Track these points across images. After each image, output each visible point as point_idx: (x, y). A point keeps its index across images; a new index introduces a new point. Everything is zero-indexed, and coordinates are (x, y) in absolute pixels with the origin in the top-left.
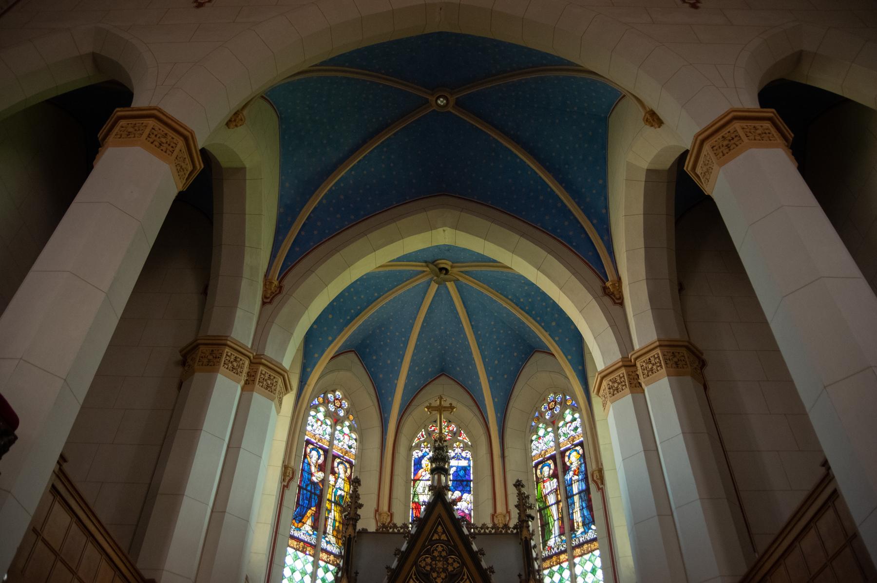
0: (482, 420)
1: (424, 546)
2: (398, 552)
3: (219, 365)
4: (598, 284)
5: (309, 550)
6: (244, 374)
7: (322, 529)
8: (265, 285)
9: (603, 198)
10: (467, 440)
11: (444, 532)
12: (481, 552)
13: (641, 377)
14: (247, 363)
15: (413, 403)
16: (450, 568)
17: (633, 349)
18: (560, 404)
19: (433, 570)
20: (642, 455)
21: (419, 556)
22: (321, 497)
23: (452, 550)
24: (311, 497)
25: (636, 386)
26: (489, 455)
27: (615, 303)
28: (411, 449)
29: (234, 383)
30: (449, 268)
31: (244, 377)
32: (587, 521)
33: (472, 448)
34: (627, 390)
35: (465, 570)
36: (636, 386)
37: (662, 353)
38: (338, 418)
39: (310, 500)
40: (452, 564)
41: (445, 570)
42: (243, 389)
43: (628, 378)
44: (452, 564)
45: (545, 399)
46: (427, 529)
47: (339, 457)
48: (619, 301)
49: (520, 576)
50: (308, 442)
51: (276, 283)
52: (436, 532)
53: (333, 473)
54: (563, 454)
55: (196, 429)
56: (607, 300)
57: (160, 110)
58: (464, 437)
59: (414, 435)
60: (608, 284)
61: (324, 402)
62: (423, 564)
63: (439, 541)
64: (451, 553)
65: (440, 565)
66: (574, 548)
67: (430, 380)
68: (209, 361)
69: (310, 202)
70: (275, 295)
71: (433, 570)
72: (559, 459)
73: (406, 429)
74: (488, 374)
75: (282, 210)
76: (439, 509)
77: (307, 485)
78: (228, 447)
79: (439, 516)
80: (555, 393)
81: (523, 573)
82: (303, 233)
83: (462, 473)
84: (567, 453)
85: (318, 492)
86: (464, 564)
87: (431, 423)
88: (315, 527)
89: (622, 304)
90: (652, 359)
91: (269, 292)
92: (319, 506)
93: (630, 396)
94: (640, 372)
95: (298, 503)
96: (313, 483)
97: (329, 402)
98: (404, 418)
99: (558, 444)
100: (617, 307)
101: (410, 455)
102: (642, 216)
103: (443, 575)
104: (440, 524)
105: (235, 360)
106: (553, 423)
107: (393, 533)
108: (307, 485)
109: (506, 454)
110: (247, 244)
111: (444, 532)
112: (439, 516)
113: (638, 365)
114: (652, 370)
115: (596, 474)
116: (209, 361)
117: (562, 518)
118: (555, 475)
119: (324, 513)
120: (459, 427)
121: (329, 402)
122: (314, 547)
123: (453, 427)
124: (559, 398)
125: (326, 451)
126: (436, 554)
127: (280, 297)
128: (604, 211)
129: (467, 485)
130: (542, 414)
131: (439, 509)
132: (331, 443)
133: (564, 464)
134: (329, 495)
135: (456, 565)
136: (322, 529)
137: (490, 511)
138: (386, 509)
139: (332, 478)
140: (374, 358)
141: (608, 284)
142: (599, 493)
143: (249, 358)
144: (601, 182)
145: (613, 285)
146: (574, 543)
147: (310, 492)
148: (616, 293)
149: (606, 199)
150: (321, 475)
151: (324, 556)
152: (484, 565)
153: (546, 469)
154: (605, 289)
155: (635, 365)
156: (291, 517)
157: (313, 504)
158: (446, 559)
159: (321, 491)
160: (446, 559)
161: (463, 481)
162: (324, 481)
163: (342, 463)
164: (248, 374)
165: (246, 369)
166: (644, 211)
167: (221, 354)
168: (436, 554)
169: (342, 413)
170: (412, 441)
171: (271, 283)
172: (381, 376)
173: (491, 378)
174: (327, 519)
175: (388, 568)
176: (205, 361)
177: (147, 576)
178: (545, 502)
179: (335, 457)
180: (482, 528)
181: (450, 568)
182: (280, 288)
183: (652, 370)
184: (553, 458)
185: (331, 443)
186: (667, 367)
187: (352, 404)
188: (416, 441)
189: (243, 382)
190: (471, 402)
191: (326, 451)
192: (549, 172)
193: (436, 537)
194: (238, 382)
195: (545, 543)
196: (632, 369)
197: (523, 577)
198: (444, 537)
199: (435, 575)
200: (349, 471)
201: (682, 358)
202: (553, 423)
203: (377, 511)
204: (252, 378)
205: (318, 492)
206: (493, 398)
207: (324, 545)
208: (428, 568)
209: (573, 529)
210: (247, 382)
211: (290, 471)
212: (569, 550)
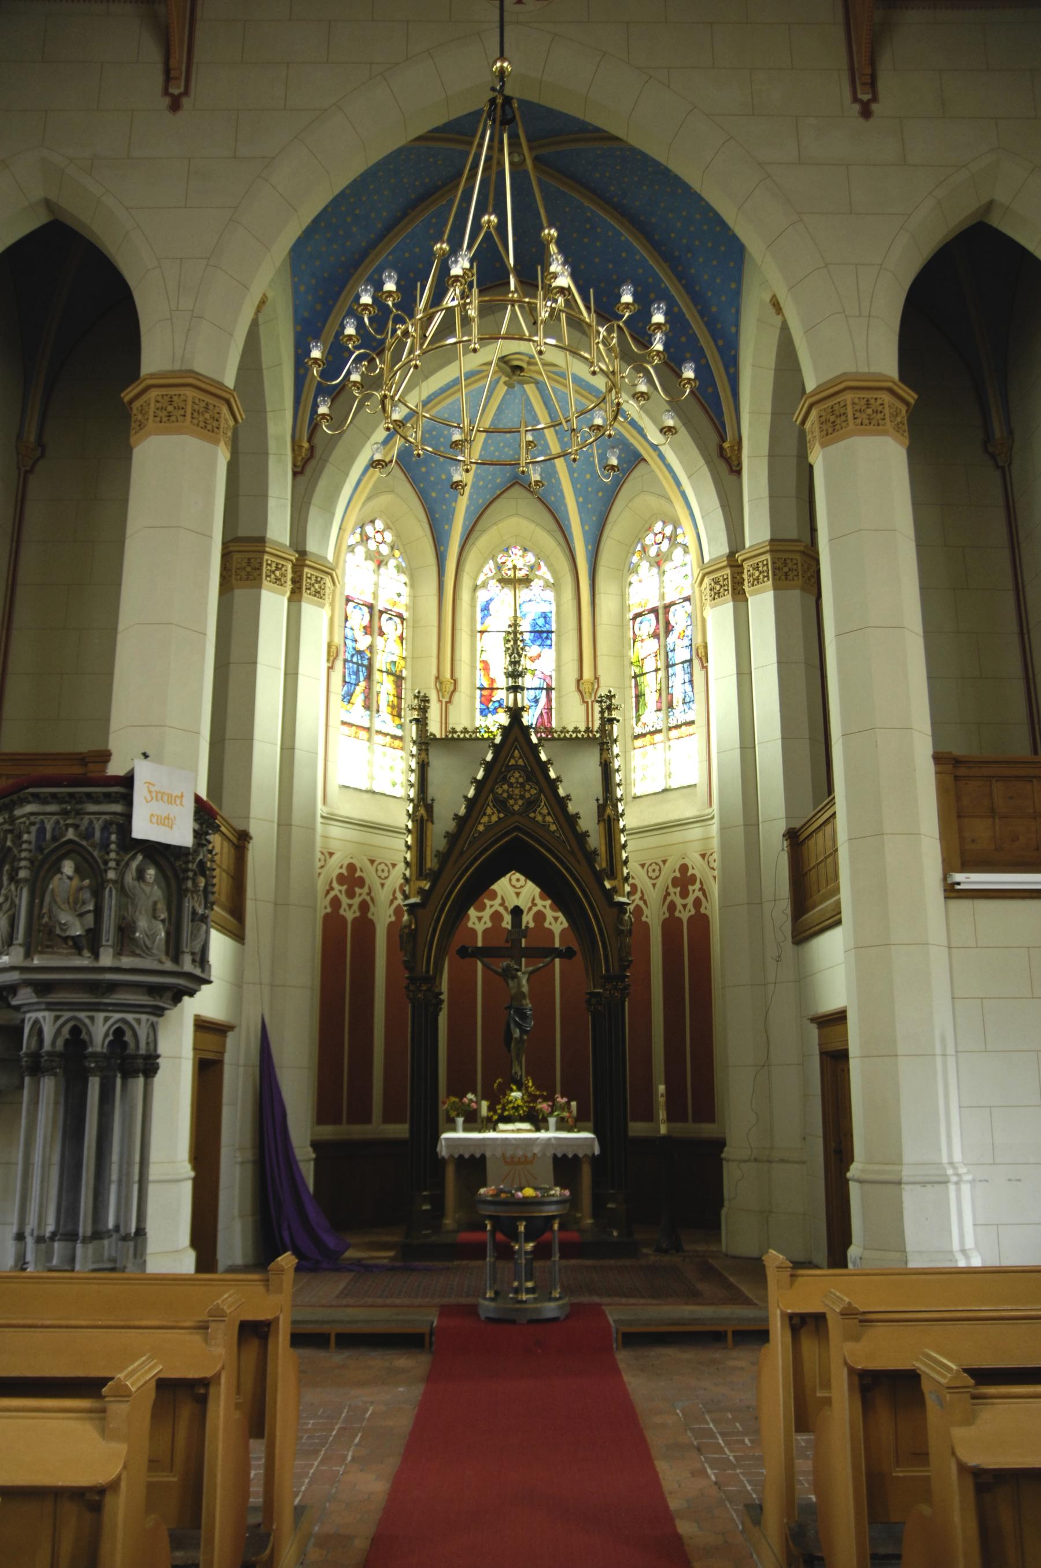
0: (567, 551)
1: (500, 772)
2: (475, 780)
3: (261, 579)
4: (713, 439)
5: (364, 734)
6: (289, 583)
7: (375, 708)
8: (293, 450)
9: (733, 310)
10: (549, 576)
11: (521, 757)
12: (558, 779)
13: (746, 582)
14: (289, 566)
15: (478, 527)
16: (527, 795)
17: (744, 548)
18: (670, 539)
19: (510, 797)
20: (735, 677)
21: (496, 783)
22: (370, 668)
23: (530, 777)
24: (358, 670)
25: (739, 595)
26: (575, 602)
27: (855, 99)
28: (475, 588)
29: (281, 597)
30: (524, 365)
31: (289, 586)
32: (688, 699)
33: (555, 586)
34: (729, 597)
35: (542, 796)
36: (739, 595)
37: (772, 559)
38: (381, 558)
39: (357, 673)
40: (529, 791)
41: (522, 797)
42: (290, 600)
43: (733, 581)
44: (529, 791)
45: (650, 529)
46: (503, 755)
47: (386, 611)
48: (736, 470)
49: (597, 800)
50: (348, 600)
51: (306, 445)
52: (512, 757)
53: (381, 633)
54: (667, 608)
55: (252, 662)
56: (723, 467)
57: (191, 371)
58: (544, 571)
59: (479, 571)
60: (726, 445)
61: (362, 540)
62: (500, 791)
63: (516, 767)
64: (528, 780)
65: (517, 791)
66: (670, 729)
67: (498, 492)
68: (248, 574)
69: (335, 311)
70: (306, 462)
71: (510, 797)
72: (662, 612)
73: (469, 567)
74: (577, 493)
75: (299, 328)
76: (516, 731)
77: (352, 656)
78: (286, 674)
79: (516, 740)
80: (664, 523)
81: (601, 798)
82: (319, 325)
83: (541, 622)
84: (672, 609)
85: (366, 662)
86: (541, 791)
87: (501, 552)
88: (367, 707)
89: (739, 472)
90: (760, 564)
91: (299, 458)
92: (369, 678)
93: (731, 605)
94: (745, 576)
95: (345, 682)
96: (360, 653)
97: (368, 538)
98: (464, 554)
99: (662, 596)
100: (734, 477)
101: (473, 599)
102: (772, 372)
103: (520, 802)
104: (516, 748)
105: (277, 569)
106: (658, 562)
107: (465, 739)
108: (352, 656)
109: (597, 601)
110: (268, 409)
111: (521, 757)
112: (516, 740)
113: (746, 565)
114: (758, 579)
115: (701, 650)
116: (248, 574)
117: (660, 690)
118: (655, 635)
119: (376, 688)
120: (538, 557)
121: (368, 538)
122: (368, 729)
123: (531, 558)
124: (668, 530)
125: (371, 607)
126: (513, 780)
127: (312, 463)
128: (733, 330)
129: (547, 638)
130: (644, 549)
131: (516, 731)
132: (375, 595)
133: (667, 623)
134: (380, 662)
135: (533, 792)
136: (375, 708)
137: (575, 675)
138: (448, 675)
139: (379, 640)
140: (423, 469)
141: (726, 445)
142: (703, 672)
143: (291, 561)
144: (733, 286)
145: (732, 447)
146: (673, 723)
147: (357, 663)
148: (734, 458)
149: (738, 312)
150: (368, 638)
151: (378, 739)
152: (562, 792)
153: (645, 624)
154: (721, 449)
155: (742, 566)
156: (341, 698)
157: (362, 678)
158: (522, 785)
159: (370, 660)
160: (522, 785)
161: (543, 632)
162: (371, 648)
163: (390, 619)
164: (293, 581)
165: (289, 575)
166: (777, 364)
167: (261, 564)
168: (513, 780)
169: (385, 550)
170: (476, 578)
171: (301, 447)
172: (434, 494)
173: (581, 499)
174: (378, 693)
175: (465, 797)
176: (243, 574)
177: (241, 828)
178: (642, 667)
179: (381, 612)
180: (562, 732)
181: (527, 795)
182: (312, 448)
183: (758, 579)
184: (654, 611)
185: (375, 595)
186: (774, 579)
187: (398, 535)
188: (481, 578)
189: (288, 594)
190: (553, 526)
191: (371, 607)
192: (666, 261)
193: (512, 762)
194: (284, 595)
195: (638, 719)
196: (738, 570)
197: (601, 802)
198: (521, 762)
199: (512, 802)
200: (400, 626)
201: (795, 567)
202: (658, 562)
203: (437, 678)
204: (298, 585)
205: (366, 662)
206: (583, 523)
207: (378, 725)
208: (505, 795)
209: (670, 706)
210: (293, 592)
211: (333, 649)
212: (664, 730)
